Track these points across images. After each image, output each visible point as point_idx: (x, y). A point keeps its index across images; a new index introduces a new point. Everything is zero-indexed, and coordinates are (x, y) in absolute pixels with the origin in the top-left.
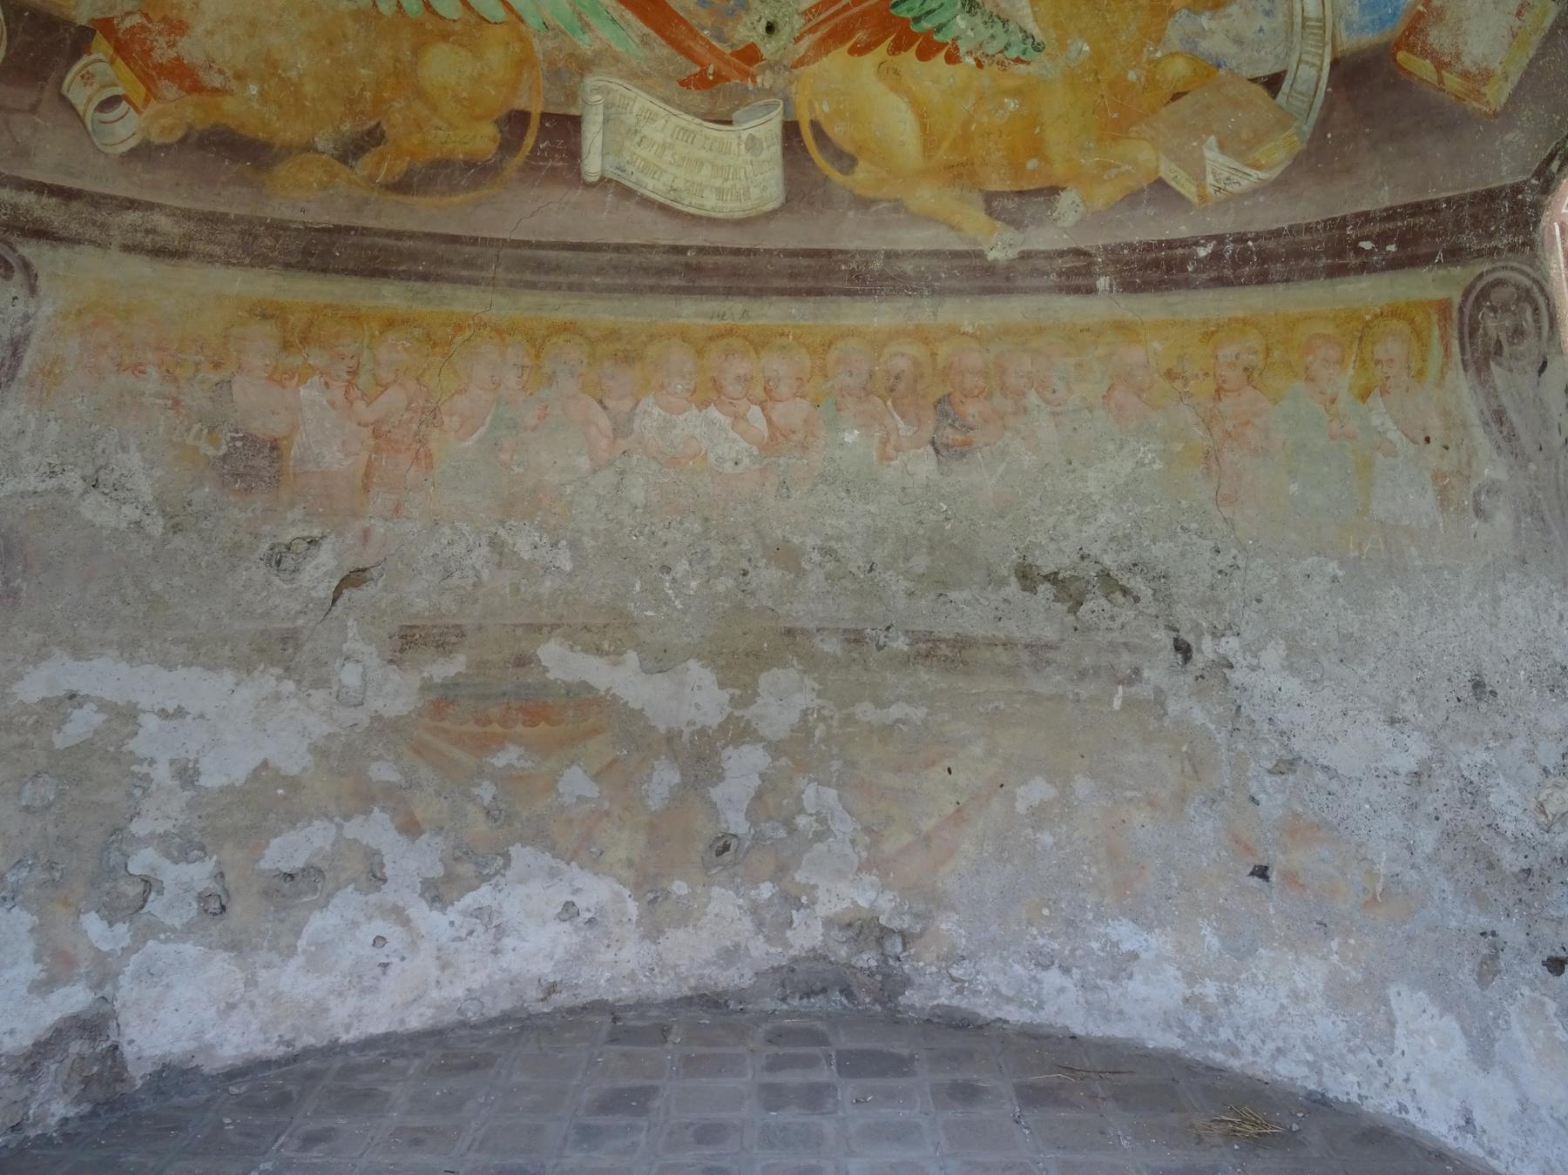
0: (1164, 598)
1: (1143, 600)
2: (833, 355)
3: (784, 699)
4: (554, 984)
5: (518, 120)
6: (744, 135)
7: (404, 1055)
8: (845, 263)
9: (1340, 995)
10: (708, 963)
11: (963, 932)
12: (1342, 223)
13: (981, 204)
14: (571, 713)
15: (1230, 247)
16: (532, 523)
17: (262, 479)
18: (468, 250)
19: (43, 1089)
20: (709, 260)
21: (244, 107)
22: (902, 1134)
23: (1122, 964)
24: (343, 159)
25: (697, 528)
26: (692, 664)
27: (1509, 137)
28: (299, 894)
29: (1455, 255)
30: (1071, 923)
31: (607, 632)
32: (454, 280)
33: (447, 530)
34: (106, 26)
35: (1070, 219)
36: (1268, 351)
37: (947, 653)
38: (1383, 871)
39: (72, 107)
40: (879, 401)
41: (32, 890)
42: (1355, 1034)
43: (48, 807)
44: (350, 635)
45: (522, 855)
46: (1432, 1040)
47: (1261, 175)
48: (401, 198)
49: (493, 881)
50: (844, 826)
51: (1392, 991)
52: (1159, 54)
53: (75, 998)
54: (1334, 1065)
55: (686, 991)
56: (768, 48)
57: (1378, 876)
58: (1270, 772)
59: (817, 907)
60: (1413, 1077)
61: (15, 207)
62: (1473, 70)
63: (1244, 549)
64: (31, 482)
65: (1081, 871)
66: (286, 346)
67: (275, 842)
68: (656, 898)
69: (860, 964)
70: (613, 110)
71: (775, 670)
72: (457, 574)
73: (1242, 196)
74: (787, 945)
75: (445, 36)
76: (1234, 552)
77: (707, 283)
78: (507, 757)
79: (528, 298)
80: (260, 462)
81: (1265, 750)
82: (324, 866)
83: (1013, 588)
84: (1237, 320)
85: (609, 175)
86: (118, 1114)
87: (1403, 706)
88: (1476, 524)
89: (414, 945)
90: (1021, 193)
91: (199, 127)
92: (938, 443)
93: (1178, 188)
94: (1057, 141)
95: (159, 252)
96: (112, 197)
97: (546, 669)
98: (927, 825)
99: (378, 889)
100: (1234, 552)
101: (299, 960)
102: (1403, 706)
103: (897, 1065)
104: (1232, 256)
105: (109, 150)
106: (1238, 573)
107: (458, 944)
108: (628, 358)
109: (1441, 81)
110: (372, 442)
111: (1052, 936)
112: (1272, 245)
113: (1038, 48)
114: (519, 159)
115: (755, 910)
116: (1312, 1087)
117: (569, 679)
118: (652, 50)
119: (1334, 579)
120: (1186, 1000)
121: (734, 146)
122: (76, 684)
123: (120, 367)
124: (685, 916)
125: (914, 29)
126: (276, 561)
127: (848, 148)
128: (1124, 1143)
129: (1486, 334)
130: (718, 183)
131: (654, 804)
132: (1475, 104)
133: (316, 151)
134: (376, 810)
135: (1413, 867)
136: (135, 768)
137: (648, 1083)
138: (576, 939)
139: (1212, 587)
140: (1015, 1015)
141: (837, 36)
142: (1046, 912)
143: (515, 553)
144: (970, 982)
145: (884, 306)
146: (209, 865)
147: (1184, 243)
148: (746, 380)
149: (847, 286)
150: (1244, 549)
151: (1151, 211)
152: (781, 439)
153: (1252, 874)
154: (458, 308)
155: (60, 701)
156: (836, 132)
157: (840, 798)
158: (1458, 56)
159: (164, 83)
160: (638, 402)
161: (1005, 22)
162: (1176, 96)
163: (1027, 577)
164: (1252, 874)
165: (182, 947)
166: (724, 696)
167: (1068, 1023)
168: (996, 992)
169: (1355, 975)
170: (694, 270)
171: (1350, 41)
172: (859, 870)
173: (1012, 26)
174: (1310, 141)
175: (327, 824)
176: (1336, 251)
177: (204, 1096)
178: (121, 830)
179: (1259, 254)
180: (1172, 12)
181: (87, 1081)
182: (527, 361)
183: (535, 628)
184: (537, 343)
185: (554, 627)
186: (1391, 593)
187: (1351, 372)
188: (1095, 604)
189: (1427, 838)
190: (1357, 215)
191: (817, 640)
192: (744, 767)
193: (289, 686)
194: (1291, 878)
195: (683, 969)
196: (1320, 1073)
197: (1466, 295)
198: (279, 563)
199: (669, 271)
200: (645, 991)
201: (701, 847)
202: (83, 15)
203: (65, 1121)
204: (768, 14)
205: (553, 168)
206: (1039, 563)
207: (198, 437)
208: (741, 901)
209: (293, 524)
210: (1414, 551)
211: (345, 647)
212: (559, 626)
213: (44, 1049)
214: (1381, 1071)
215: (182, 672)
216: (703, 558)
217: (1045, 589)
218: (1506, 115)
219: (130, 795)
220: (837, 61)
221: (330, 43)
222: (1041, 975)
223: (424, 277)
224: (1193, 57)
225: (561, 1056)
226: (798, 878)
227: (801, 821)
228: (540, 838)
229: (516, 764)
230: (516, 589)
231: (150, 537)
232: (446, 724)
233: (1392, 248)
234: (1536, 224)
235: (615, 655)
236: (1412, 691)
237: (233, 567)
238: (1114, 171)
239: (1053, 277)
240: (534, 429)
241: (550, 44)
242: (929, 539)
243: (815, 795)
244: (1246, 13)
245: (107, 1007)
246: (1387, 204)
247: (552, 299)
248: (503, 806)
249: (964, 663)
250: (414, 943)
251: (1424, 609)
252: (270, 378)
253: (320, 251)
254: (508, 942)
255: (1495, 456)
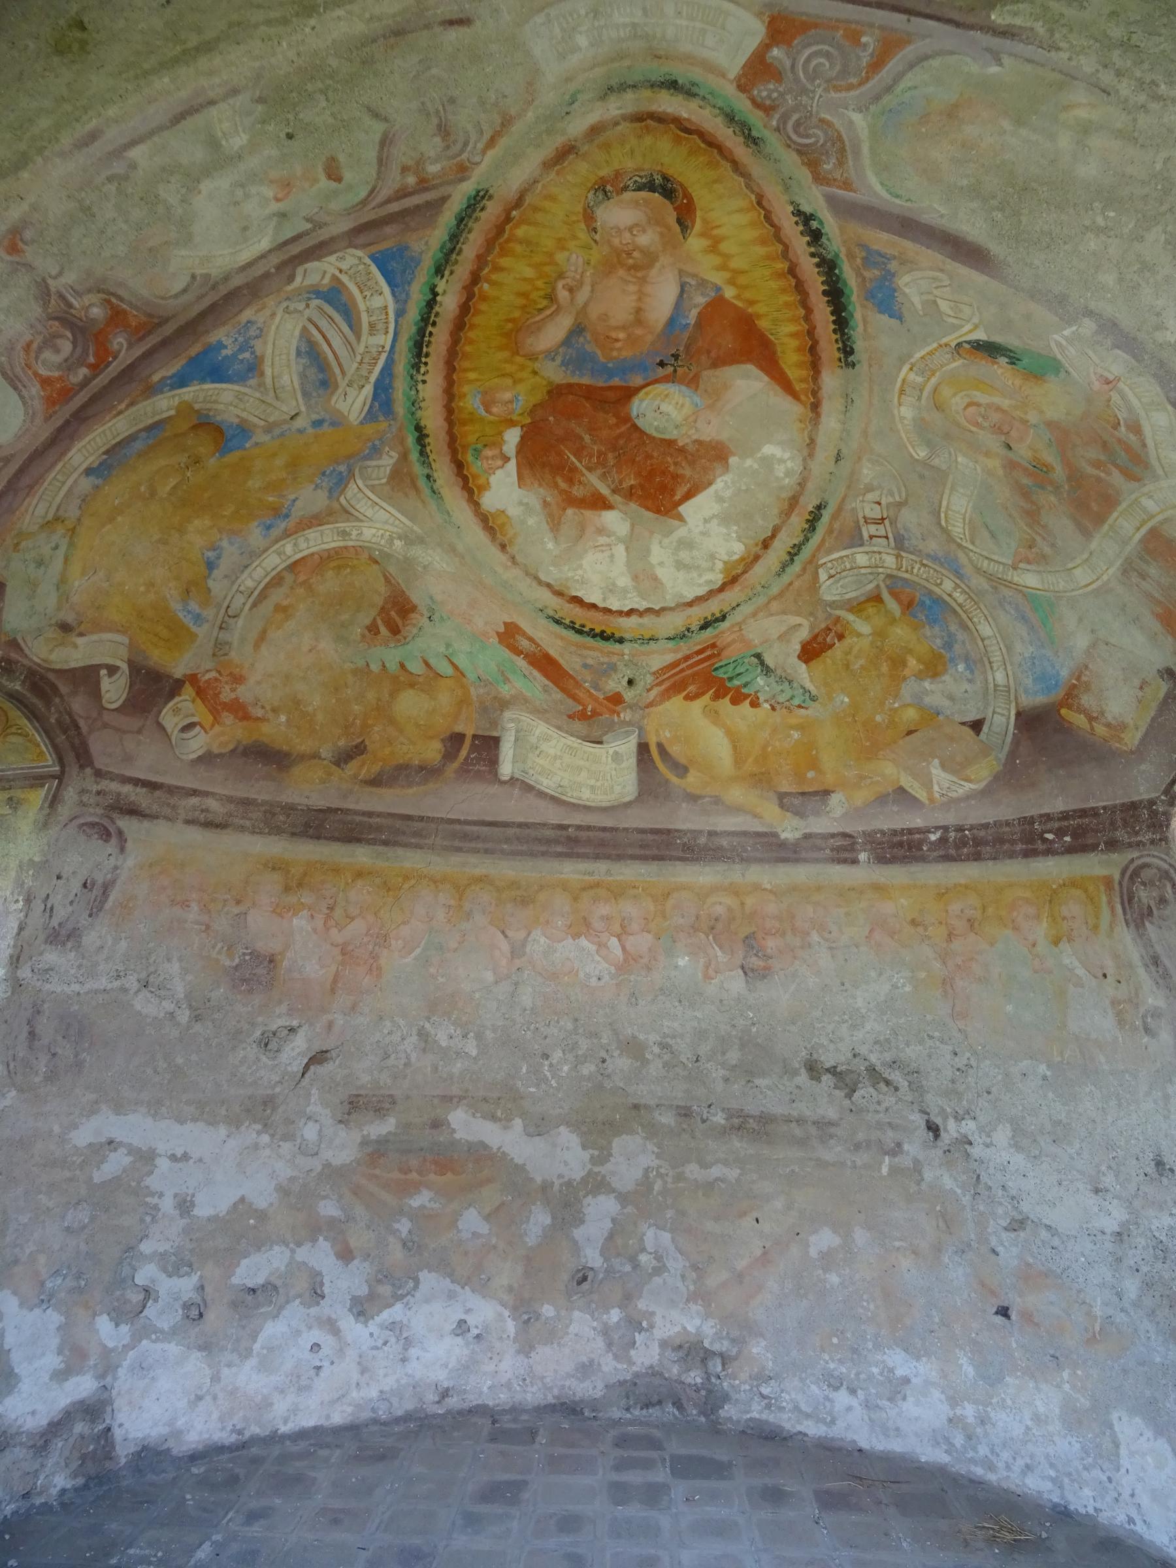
0: (917, 1088)
1: (901, 1090)
2: (671, 902)
3: (632, 1158)
4: (447, 1390)
5: (456, 739)
6: (611, 751)
7: (328, 1446)
8: (680, 838)
9: (1073, 1419)
10: (569, 1376)
11: (769, 1355)
12: (1031, 821)
13: (776, 801)
14: (470, 1165)
15: (952, 834)
16: (449, 1019)
17: (260, 983)
18: (418, 825)
19: (50, 1463)
20: (584, 834)
21: (275, 730)
22: (722, 1530)
23: (897, 1388)
24: (337, 763)
25: (570, 1026)
26: (562, 1129)
27: (1143, 767)
28: (258, 1306)
29: (1112, 845)
30: (855, 1351)
31: (500, 1103)
32: (406, 845)
33: (388, 1024)
34: (193, 679)
35: (838, 812)
36: (984, 908)
37: (754, 1126)
38: (1099, 1313)
39: (164, 729)
40: (702, 936)
41: (63, 1294)
42: (1087, 1454)
43: (84, 1227)
44: (313, 1100)
45: (428, 1279)
46: (1150, 1460)
47: (972, 786)
48: (374, 789)
49: (405, 1301)
50: (676, 1264)
51: (1115, 1416)
52: (896, 705)
53: (83, 1386)
54: (1073, 1481)
55: (550, 1399)
56: (629, 695)
57: (1096, 1317)
58: (1006, 1229)
59: (655, 1331)
60: (1137, 1492)
61: (119, 794)
62: (1113, 722)
63: (975, 1053)
64: (103, 983)
65: (862, 1307)
66: (287, 889)
67: (244, 1262)
68: (529, 1319)
69: (689, 1380)
70: (522, 733)
71: (624, 1136)
72: (393, 1056)
73: (958, 800)
74: (631, 1363)
75: (412, 685)
76: (968, 1055)
77: (582, 850)
78: (421, 1200)
79: (456, 859)
80: (261, 971)
81: (1000, 1211)
82: (278, 1283)
83: (803, 1078)
84: (960, 885)
85: (517, 776)
86: (105, 1488)
87: (1103, 1179)
88: (1146, 1040)
89: (341, 1352)
90: (803, 794)
91: (244, 743)
92: (746, 967)
93: (913, 793)
94: (828, 760)
95: (208, 825)
96: (183, 788)
97: (454, 1131)
98: (741, 1264)
99: (318, 1304)
100: (968, 1055)
101: (253, 1362)
102: (1103, 1179)
103: (718, 1470)
104: (954, 841)
105: (184, 757)
106: (971, 1071)
107: (375, 1352)
108: (524, 902)
109: (1092, 728)
110: (340, 958)
111: (841, 1361)
112: (982, 833)
113: (813, 699)
114: (456, 765)
115: (606, 1332)
116: (1056, 1500)
117: (470, 1138)
118: (550, 695)
119: (1045, 1078)
120: (950, 1420)
121: (604, 758)
122: (118, 1135)
123: (173, 902)
124: (552, 1336)
125: (729, 685)
126: (265, 1044)
127: (683, 761)
128: (904, 1544)
129: (1140, 900)
130: (592, 782)
131: (531, 1240)
132: (1118, 745)
133: (320, 758)
134: (321, 1238)
135: (1122, 1310)
136: (148, 1199)
137: (519, 1477)
138: (466, 1352)
139: (953, 1081)
140: (813, 1429)
141: (677, 688)
142: (835, 1340)
143: (436, 1041)
144: (776, 1400)
145: (707, 869)
146: (195, 1278)
147: (919, 831)
148: (607, 919)
149: (681, 854)
150: (975, 1053)
151: (895, 809)
152: (632, 962)
153: (997, 1313)
154: (407, 865)
155: (101, 1145)
156: (674, 750)
157: (673, 1240)
158: (1102, 713)
159: (225, 714)
160: (529, 934)
161: (790, 682)
162: (910, 733)
163: (813, 1069)
164: (997, 1313)
165: (166, 1346)
166: (586, 1155)
167: (855, 1437)
168: (797, 1408)
169: (1084, 1402)
170: (575, 841)
171: (1027, 701)
172: (688, 1300)
173: (795, 685)
174: (1005, 765)
175: (283, 1248)
176: (1029, 839)
177: (170, 1476)
178: (132, 1248)
179: (974, 839)
180: (905, 679)
181: (83, 1458)
182: (452, 902)
183: (447, 1099)
184: (460, 890)
185: (461, 1098)
186: (1088, 1090)
187: (1045, 925)
188: (865, 1092)
189: (1131, 1287)
190: (1041, 816)
191: (656, 1114)
192: (600, 1212)
193: (265, 1138)
194: (1028, 1317)
195: (548, 1380)
196: (1061, 1487)
197: (1123, 873)
198: (266, 1045)
199: (557, 841)
200: (518, 1397)
201: (565, 1277)
202: (179, 672)
203: (64, 1491)
204: (629, 673)
205: (479, 771)
206: (822, 1059)
207: (219, 953)
208: (595, 1324)
209: (279, 1016)
210: (1102, 1059)
211: (308, 1109)
212: (465, 1098)
213: (56, 1427)
214: (1111, 1486)
215: (190, 1126)
216: (573, 1049)
217: (827, 1079)
218: (1139, 753)
219: (142, 1221)
220: (676, 703)
221: (336, 689)
222: (833, 1395)
223: (385, 843)
224: (920, 707)
225: (451, 1451)
226: (640, 1306)
227: (643, 1258)
228: (443, 1266)
229: (428, 1205)
230: (435, 1069)
231: (179, 1024)
232: (377, 1172)
233: (1068, 839)
234: (1168, 826)
235: (505, 1122)
236: (1110, 1167)
237: (234, 1048)
238: (869, 781)
239: (828, 851)
240: (455, 950)
241: (482, 691)
242: (740, 1039)
243: (652, 1237)
244: (955, 680)
245: (106, 1395)
246: (1062, 809)
247: (473, 859)
248: (416, 1239)
249: (767, 1134)
250: (341, 1350)
251: (1113, 1103)
252: (274, 911)
253: (316, 825)
254: (413, 1352)
255: (1155, 989)
